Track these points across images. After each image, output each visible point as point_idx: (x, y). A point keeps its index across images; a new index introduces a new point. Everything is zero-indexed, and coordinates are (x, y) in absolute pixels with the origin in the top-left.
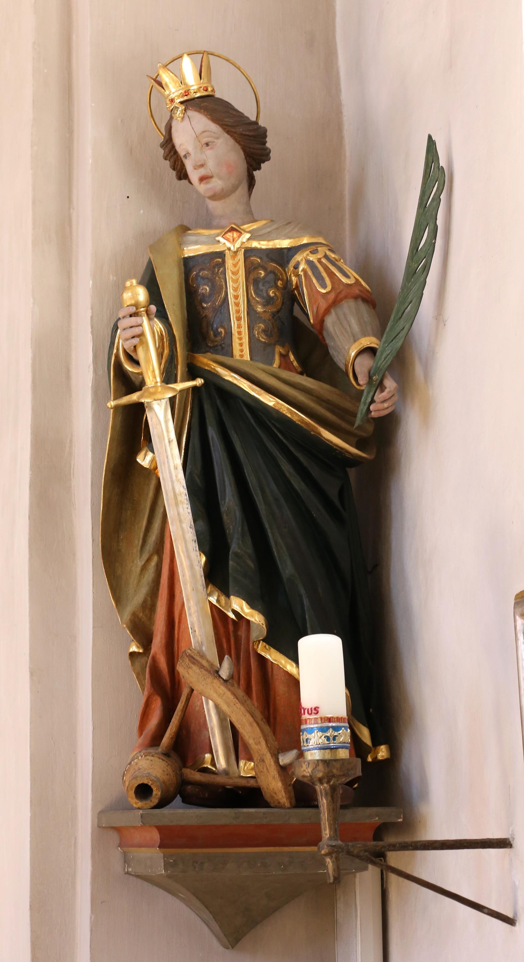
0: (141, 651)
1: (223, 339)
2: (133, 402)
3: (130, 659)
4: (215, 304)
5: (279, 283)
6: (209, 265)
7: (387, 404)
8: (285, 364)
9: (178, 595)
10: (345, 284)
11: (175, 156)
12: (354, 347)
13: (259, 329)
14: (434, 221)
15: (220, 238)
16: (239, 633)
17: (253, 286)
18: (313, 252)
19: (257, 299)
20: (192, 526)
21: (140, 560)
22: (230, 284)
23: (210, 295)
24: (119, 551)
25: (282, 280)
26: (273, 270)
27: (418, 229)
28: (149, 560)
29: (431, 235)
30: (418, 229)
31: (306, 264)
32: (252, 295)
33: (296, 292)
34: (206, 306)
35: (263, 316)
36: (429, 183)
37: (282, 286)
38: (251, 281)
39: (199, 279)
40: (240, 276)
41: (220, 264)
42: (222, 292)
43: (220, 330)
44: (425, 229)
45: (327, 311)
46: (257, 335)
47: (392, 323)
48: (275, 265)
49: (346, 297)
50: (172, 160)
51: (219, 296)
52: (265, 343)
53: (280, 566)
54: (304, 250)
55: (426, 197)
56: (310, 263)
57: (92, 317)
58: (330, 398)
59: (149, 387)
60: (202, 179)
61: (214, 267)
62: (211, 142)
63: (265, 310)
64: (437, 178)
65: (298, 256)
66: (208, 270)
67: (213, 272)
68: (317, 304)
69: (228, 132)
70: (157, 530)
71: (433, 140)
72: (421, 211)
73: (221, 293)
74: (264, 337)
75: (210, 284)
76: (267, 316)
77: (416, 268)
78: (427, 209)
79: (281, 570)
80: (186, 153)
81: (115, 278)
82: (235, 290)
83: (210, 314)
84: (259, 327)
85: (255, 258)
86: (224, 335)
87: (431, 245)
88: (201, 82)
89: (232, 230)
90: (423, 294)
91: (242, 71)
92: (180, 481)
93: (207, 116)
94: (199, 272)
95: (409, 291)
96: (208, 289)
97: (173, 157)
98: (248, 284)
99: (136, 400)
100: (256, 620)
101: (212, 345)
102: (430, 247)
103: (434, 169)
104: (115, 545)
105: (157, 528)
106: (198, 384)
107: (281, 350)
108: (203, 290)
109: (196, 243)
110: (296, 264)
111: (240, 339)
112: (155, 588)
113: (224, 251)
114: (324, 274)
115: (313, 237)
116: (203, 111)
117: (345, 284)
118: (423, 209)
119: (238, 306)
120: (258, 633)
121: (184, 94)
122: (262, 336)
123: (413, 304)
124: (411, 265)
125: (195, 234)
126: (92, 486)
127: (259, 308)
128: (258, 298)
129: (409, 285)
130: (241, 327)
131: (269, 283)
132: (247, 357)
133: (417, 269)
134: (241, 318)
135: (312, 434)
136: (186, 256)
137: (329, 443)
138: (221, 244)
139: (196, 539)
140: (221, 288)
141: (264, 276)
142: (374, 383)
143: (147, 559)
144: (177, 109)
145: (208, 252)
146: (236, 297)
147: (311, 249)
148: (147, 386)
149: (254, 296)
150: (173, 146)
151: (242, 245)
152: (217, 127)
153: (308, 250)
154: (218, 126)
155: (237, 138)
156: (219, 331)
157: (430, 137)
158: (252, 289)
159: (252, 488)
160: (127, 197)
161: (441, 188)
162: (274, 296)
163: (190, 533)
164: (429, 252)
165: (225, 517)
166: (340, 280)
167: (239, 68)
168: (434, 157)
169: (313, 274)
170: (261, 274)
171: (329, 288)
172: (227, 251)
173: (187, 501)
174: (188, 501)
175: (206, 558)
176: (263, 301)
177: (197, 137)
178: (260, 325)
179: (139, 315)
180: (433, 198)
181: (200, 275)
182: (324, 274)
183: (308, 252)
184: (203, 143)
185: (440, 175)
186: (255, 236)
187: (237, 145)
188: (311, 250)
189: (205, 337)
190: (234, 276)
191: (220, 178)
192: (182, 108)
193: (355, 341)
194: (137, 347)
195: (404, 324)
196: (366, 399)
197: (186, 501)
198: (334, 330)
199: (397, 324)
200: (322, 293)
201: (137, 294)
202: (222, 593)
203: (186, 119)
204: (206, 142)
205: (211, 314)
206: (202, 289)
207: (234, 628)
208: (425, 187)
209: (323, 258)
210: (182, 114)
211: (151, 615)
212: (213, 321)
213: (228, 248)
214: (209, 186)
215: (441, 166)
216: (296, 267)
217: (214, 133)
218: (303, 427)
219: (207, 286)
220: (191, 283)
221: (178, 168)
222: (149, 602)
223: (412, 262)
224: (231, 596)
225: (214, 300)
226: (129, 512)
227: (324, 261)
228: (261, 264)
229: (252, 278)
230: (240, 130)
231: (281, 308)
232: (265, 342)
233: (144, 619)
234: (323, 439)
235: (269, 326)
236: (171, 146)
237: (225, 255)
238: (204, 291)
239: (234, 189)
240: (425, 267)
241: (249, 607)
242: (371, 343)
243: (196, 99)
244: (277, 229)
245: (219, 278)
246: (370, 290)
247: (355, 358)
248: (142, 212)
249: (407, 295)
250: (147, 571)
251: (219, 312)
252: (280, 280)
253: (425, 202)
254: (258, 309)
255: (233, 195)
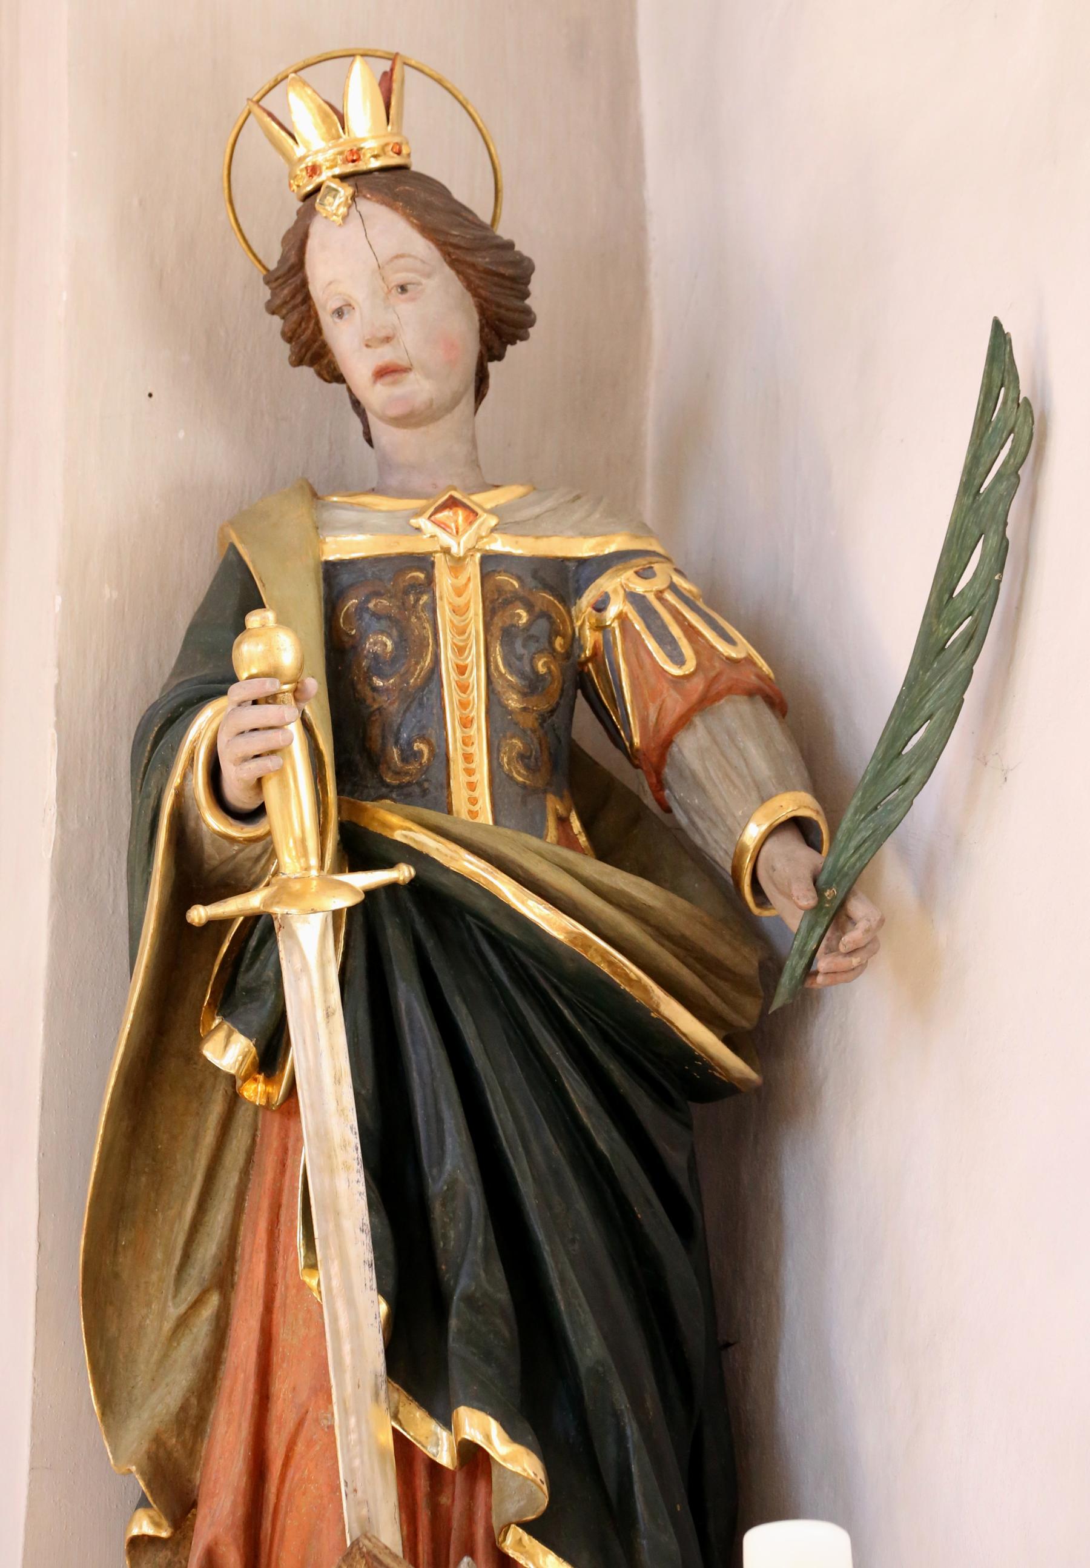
0: (164, 1534)
1: (425, 769)
2: (251, 912)
3: (129, 1552)
4: (408, 683)
5: (559, 642)
6: (393, 585)
7: (858, 959)
8: (567, 840)
9: (282, 1396)
10: (724, 659)
11: (304, 308)
12: (758, 815)
13: (511, 751)
14: (1001, 529)
15: (422, 522)
16: (444, 1500)
17: (501, 645)
18: (645, 574)
19: (509, 677)
20: (365, 1228)
21: (174, 1304)
22: (446, 638)
23: (394, 660)
24: (116, 1276)
25: (564, 636)
26: (546, 610)
27: (957, 545)
28: (197, 1304)
29: (991, 560)
30: (957, 545)
31: (627, 602)
32: (497, 667)
33: (590, 665)
34: (381, 684)
35: (520, 718)
36: (989, 438)
37: (563, 651)
38: (496, 631)
39: (367, 616)
40: (471, 620)
41: (420, 585)
42: (426, 655)
43: (418, 746)
44: (973, 544)
45: (684, 721)
46: (506, 765)
47: (879, 764)
48: (552, 598)
49: (730, 690)
50: (295, 317)
51: (417, 663)
52: (524, 786)
53: (572, 1339)
54: (620, 567)
55: (981, 469)
56: (636, 600)
57: (58, 688)
58: (688, 933)
59: (289, 879)
60: (383, 373)
61: (406, 593)
62: (413, 284)
63: (525, 705)
64: (1012, 425)
65: (608, 579)
66: (391, 597)
67: (403, 604)
68: (658, 702)
69: (454, 263)
70: (223, 1228)
71: (1006, 332)
72: (967, 501)
73: (422, 657)
74: (522, 771)
75: (395, 633)
76: (529, 721)
77: (946, 637)
78: (982, 498)
79: (575, 1349)
80: (344, 303)
81: (115, 595)
82: (460, 650)
83: (393, 707)
84: (513, 746)
85: (506, 578)
86: (429, 760)
87: (989, 586)
88: (387, 129)
89: (452, 503)
90: (963, 701)
91: (472, 110)
92: (345, 1114)
93: (412, 219)
94: (367, 600)
95: (924, 693)
96: (389, 643)
97: (296, 311)
98: (489, 638)
99: (259, 908)
100: (525, 1470)
101: (395, 782)
102: (987, 590)
103: (1004, 403)
104: (108, 1262)
105: (221, 1225)
106: (401, 878)
107: (558, 807)
108: (375, 646)
109: (358, 527)
110: (600, 599)
111: (470, 772)
112: (210, 1376)
113: (431, 554)
114: (676, 631)
115: (636, 537)
116: (402, 206)
117: (724, 659)
118: (971, 498)
119: (464, 692)
120: (522, 1503)
121: (350, 158)
122: (517, 768)
123: (935, 722)
124: (934, 629)
125: (352, 504)
126: (42, 1109)
127: (512, 699)
128: (511, 674)
129: (926, 679)
130: (473, 744)
131: (537, 641)
132: (486, 817)
133: (949, 639)
134: (472, 721)
135: (653, 1017)
136: (331, 558)
137: (687, 1041)
138: (425, 537)
139: (373, 1258)
140: (423, 645)
141: (528, 621)
142: (827, 905)
143: (193, 1300)
144: (334, 193)
145: (390, 554)
146: (462, 670)
147: (637, 566)
148: (283, 874)
149: (503, 671)
150: (304, 283)
151: (477, 543)
152: (430, 248)
153: (632, 568)
154: (432, 246)
155: (472, 278)
156: (415, 748)
157: (997, 325)
158: (498, 653)
159: (506, 1139)
160: (147, 394)
161: (1023, 449)
162: (545, 674)
163: (360, 1244)
164: (983, 601)
165: (437, 1210)
166: (713, 647)
167: (464, 103)
168: (1006, 374)
169: (649, 627)
170: (520, 616)
171: (690, 666)
172: (438, 555)
173: (358, 1164)
174: (361, 1163)
175: (389, 1311)
176: (523, 683)
177: (379, 267)
178: (514, 741)
179: (278, 700)
180: (998, 472)
181: (368, 608)
182: (676, 631)
183: (630, 573)
184: (393, 284)
185: (1021, 419)
186: (506, 524)
187: (468, 295)
188: (639, 568)
189: (375, 761)
190: (457, 617)
191: (428, 376)
192: (345, 191)
193: (763, 800)
194: (264, 781)
195: (909, 769)
196: (805, 945)
197: (355, 1163)
198: (706, 769)
199: (890, 769)
200: (670, 677)
201: (282, 648)
202: (411, 1398)
203: (355, 221)
204: (401, 282)
205: (396, 705)
206: (375, 644)
207: (432, 1486)
208: (980, 444)
209: (669, 590)
210: (345, 205)
211: (195, 1443)
212: (400, 724)
213: (442, 548)
214: (398, 391)
215: (1025, 399)
216: (600, 607)
217: (423, 262)
218: (636, 999)
219: (387, 637)
220: (342, 626)
221: (302, 337)
222: (193, 1412)
223: (939, 623)
224: (459, 1405)
225: (407, 672)
226: (144, 1179)
227: (669, 596)
228: (522, 593)
229: (500, 624)
230: (483, 260)
231: (558, 704)
232: (525, 783)
233: (179, 1453)
234: (676, 1031)
235: (532, 746)
236: (298, 282)
237: (433, 564)
238: (378, 648)
239: (455, 402)
240: (972, 638)
241: (506, 1436)
242: (799, 808)
243: (376, 174)
244: (554, 510)
245: (419, 618)
246: (772, 675)
247: (763, 840)
248: (181, 434)
249: (921, 700)
250: (187, 1331)
251: (416, 703)
252: (560, 636)
253: (977, 482)
254: (510, 702)
255: (449, 416)
